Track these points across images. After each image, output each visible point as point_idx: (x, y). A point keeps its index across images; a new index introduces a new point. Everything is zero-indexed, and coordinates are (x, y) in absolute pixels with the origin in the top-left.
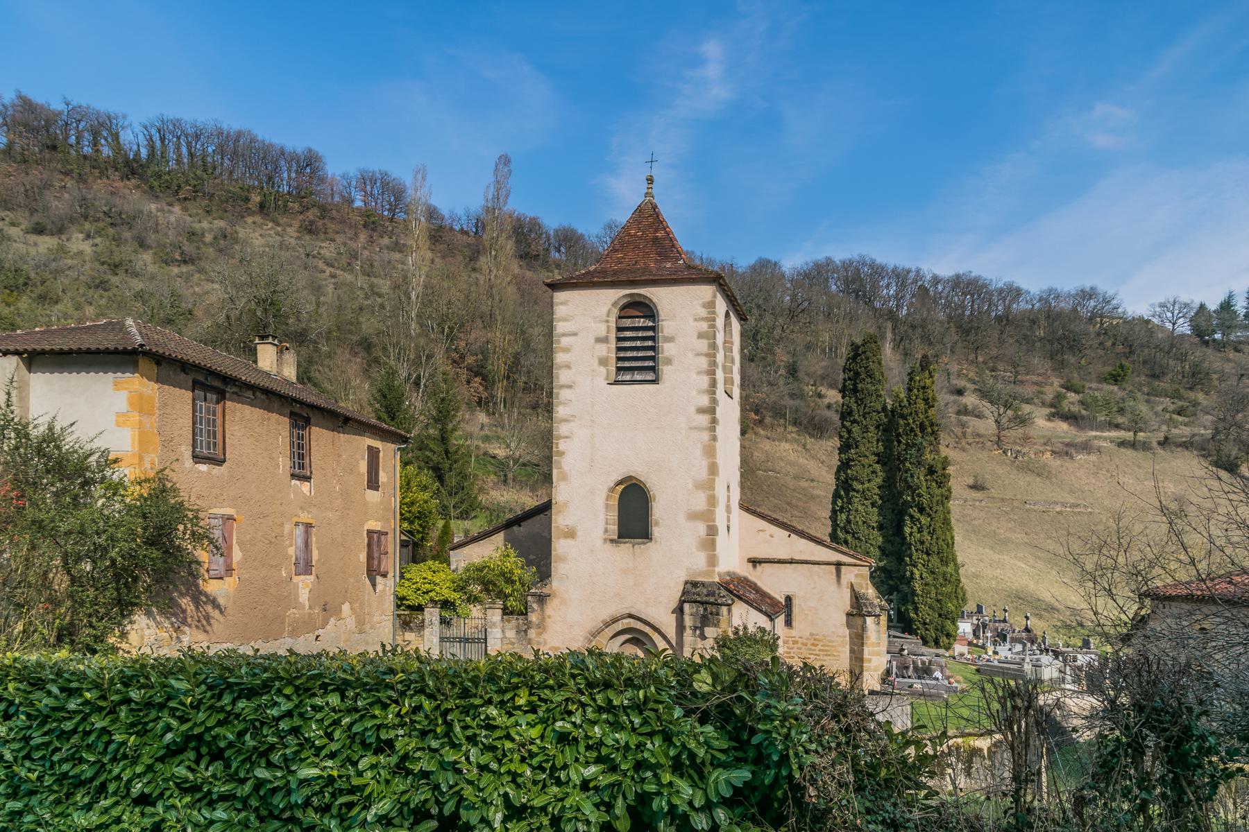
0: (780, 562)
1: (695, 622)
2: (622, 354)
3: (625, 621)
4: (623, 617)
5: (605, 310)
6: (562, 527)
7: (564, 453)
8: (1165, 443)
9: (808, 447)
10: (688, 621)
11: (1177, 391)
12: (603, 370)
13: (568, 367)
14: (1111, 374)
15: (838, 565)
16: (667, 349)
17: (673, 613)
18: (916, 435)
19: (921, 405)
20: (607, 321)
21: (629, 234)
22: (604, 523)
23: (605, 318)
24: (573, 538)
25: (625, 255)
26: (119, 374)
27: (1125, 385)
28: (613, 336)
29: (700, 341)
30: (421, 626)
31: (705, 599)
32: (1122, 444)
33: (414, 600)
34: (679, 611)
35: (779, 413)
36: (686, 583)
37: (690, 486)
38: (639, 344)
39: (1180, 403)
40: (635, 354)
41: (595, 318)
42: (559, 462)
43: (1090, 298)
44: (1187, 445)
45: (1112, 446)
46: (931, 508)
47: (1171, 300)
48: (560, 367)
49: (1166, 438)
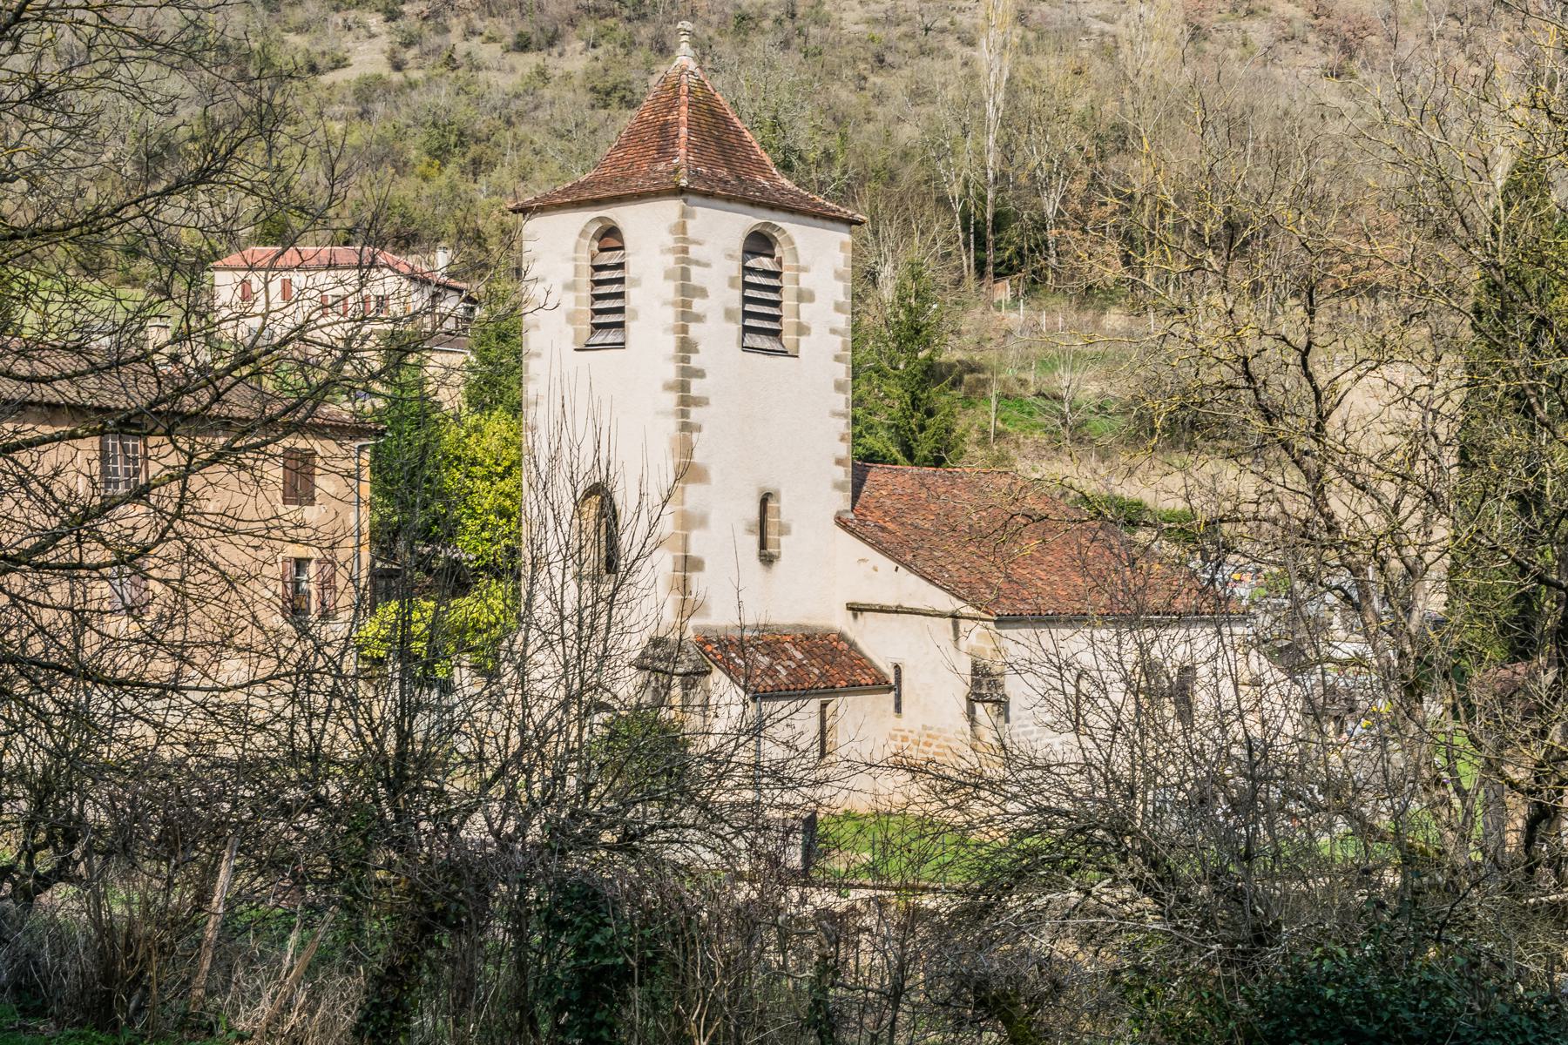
0: (882, 610)
15: (955, 617)
23: (572, 255)
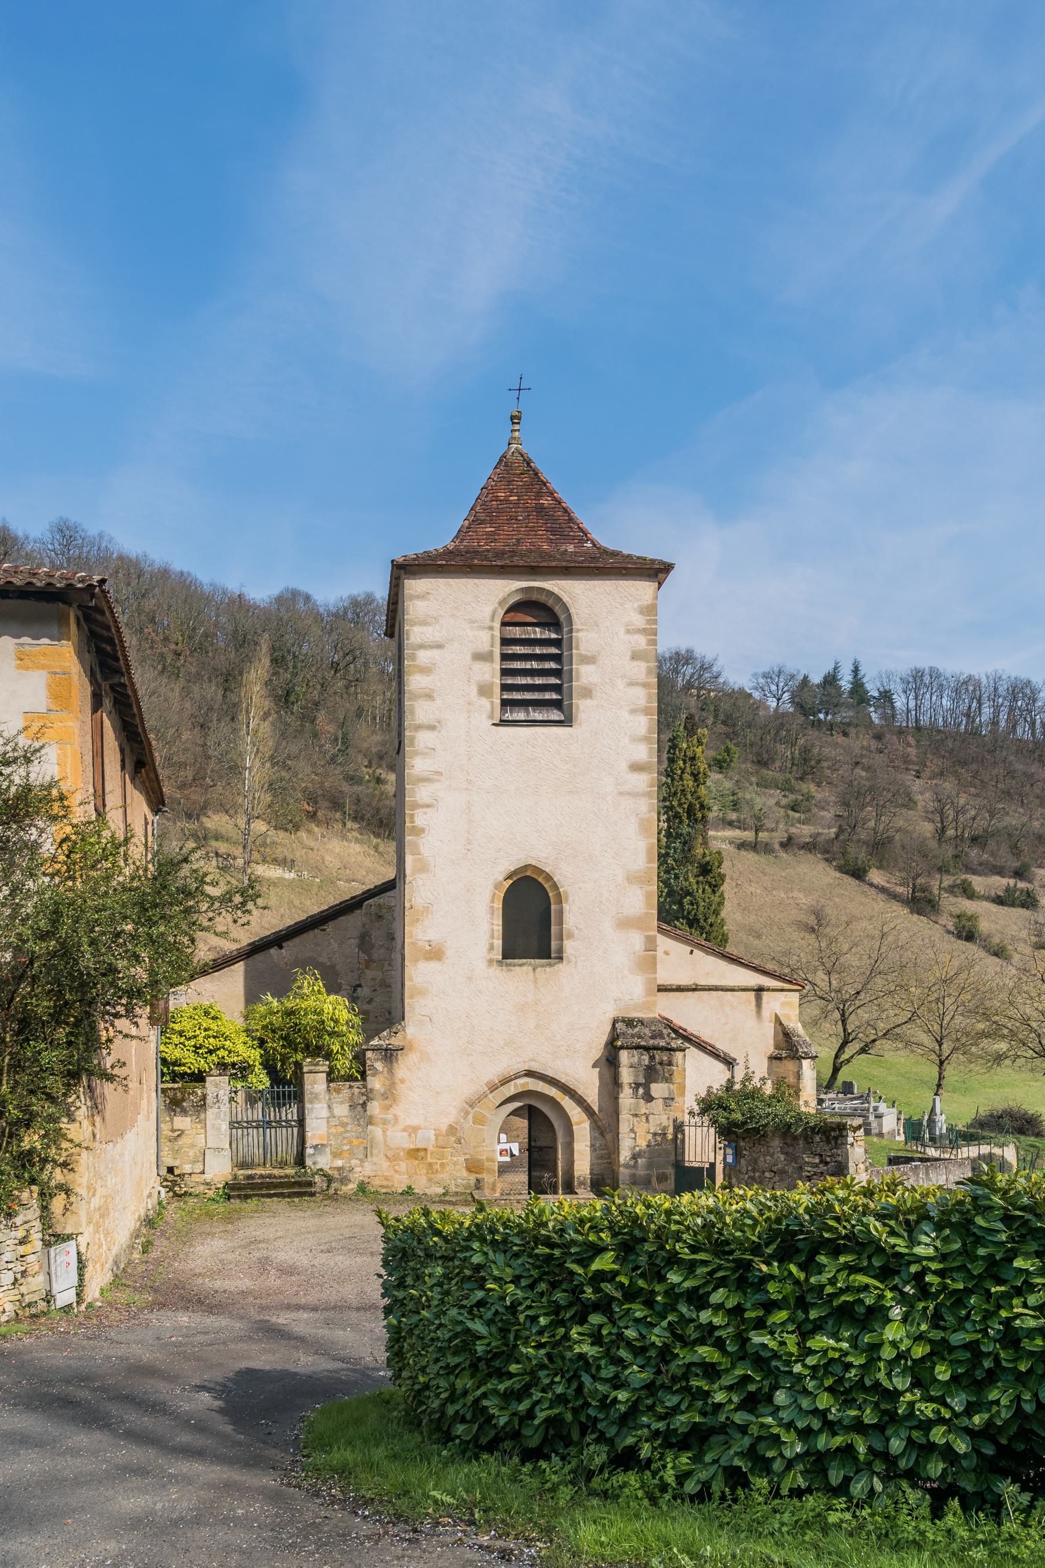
0: (679, 989)
1: (637, 1076)
3: (518, 1081)
4: (517, 1076)
5: (488, 610)
6: (420, 943)
7: (423, 830)
8: (788, 844)
9: (381, 849)
10: (626, 1076)
11: (788, 781)
12: (485, 702)
13: (429, 696)
15: (760, 990)
16: (584, 674)
17: (594, 1066)
18: (681, 822)
19: (690, 783)
21: (497, 499)
26: (26, 640)
27: (731, 773)
28: (497, 651)
29: (635, 663)
30: (202, 1105)
31: (651, 1042)
32: (742, 846)
33: (193, 1062)
34: (610, 1061)
35: (336, 804)
36: (615, 1022)
37: (620, 879)
39: (792, 797)
40: (528, 680)
42: (416, 845)
43: (687, 663)
44: (810, 847)
45: (732, 849)
46: (705, 920)
47: (776, 670)
48: (416, 697)
49: (790, 838)
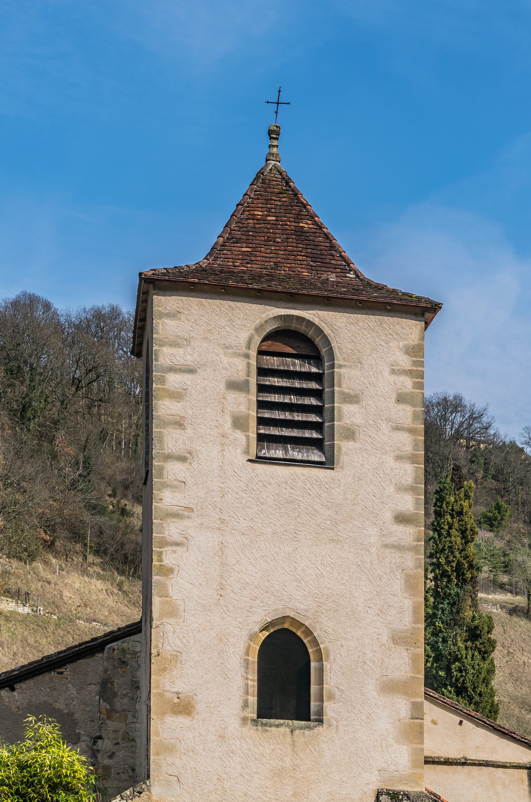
0: (448, 762)
2: (267, 414)
5: (243, 336)
7: (171, 571)
9: (125, 588)
12: (240, 435)
13: (179, 424)
14: (485, 516)
20: (247, 356)
21: (253, 217)
22: (241, 692)
24: (189, 714)
25: (254, 249)
28: (253, 381)
29: (401, 407)
37: (385, 639)
38: (293, 399)
40: (287, 416)
41: (227, 348)
42: (164, 586)
45: (503, 614)
